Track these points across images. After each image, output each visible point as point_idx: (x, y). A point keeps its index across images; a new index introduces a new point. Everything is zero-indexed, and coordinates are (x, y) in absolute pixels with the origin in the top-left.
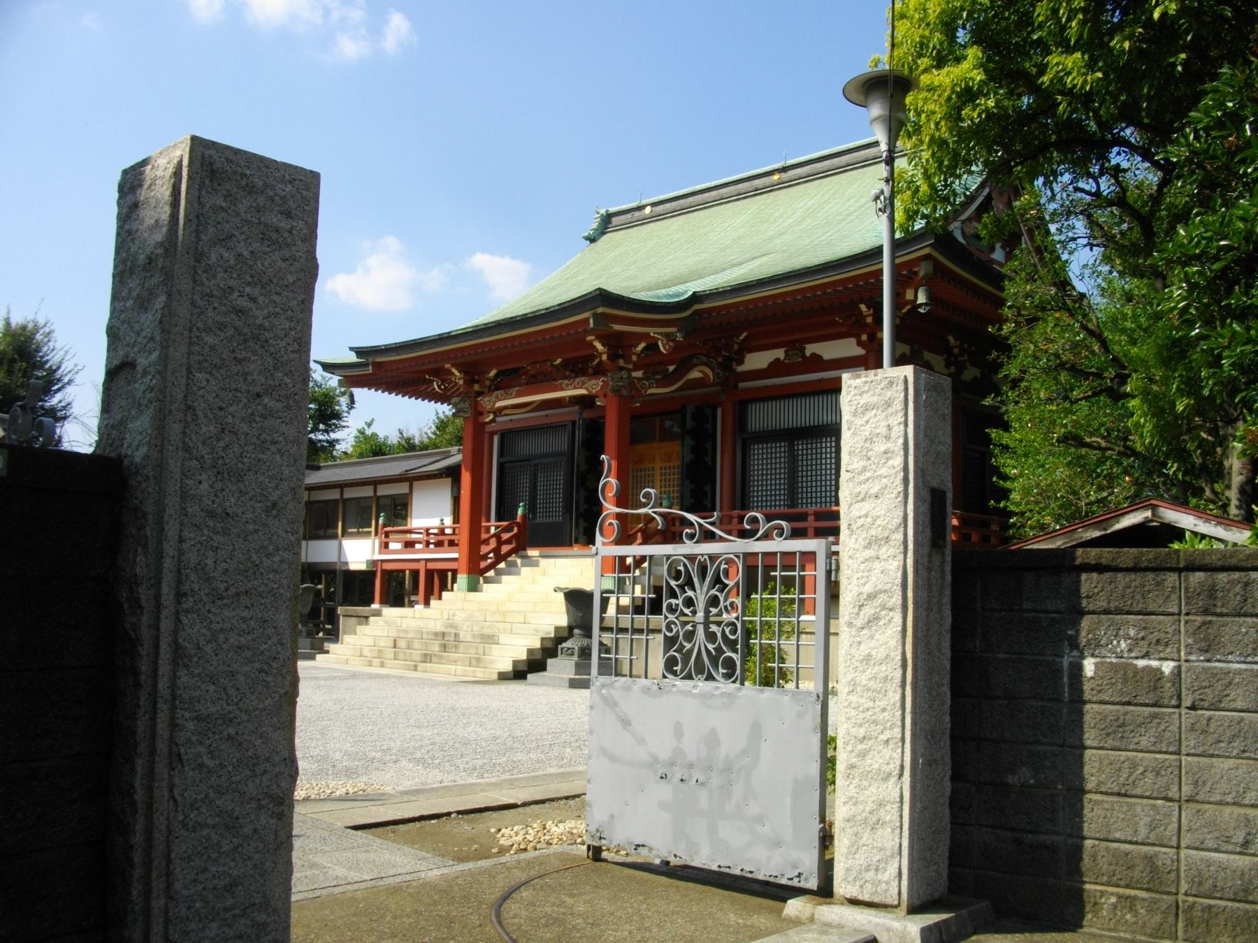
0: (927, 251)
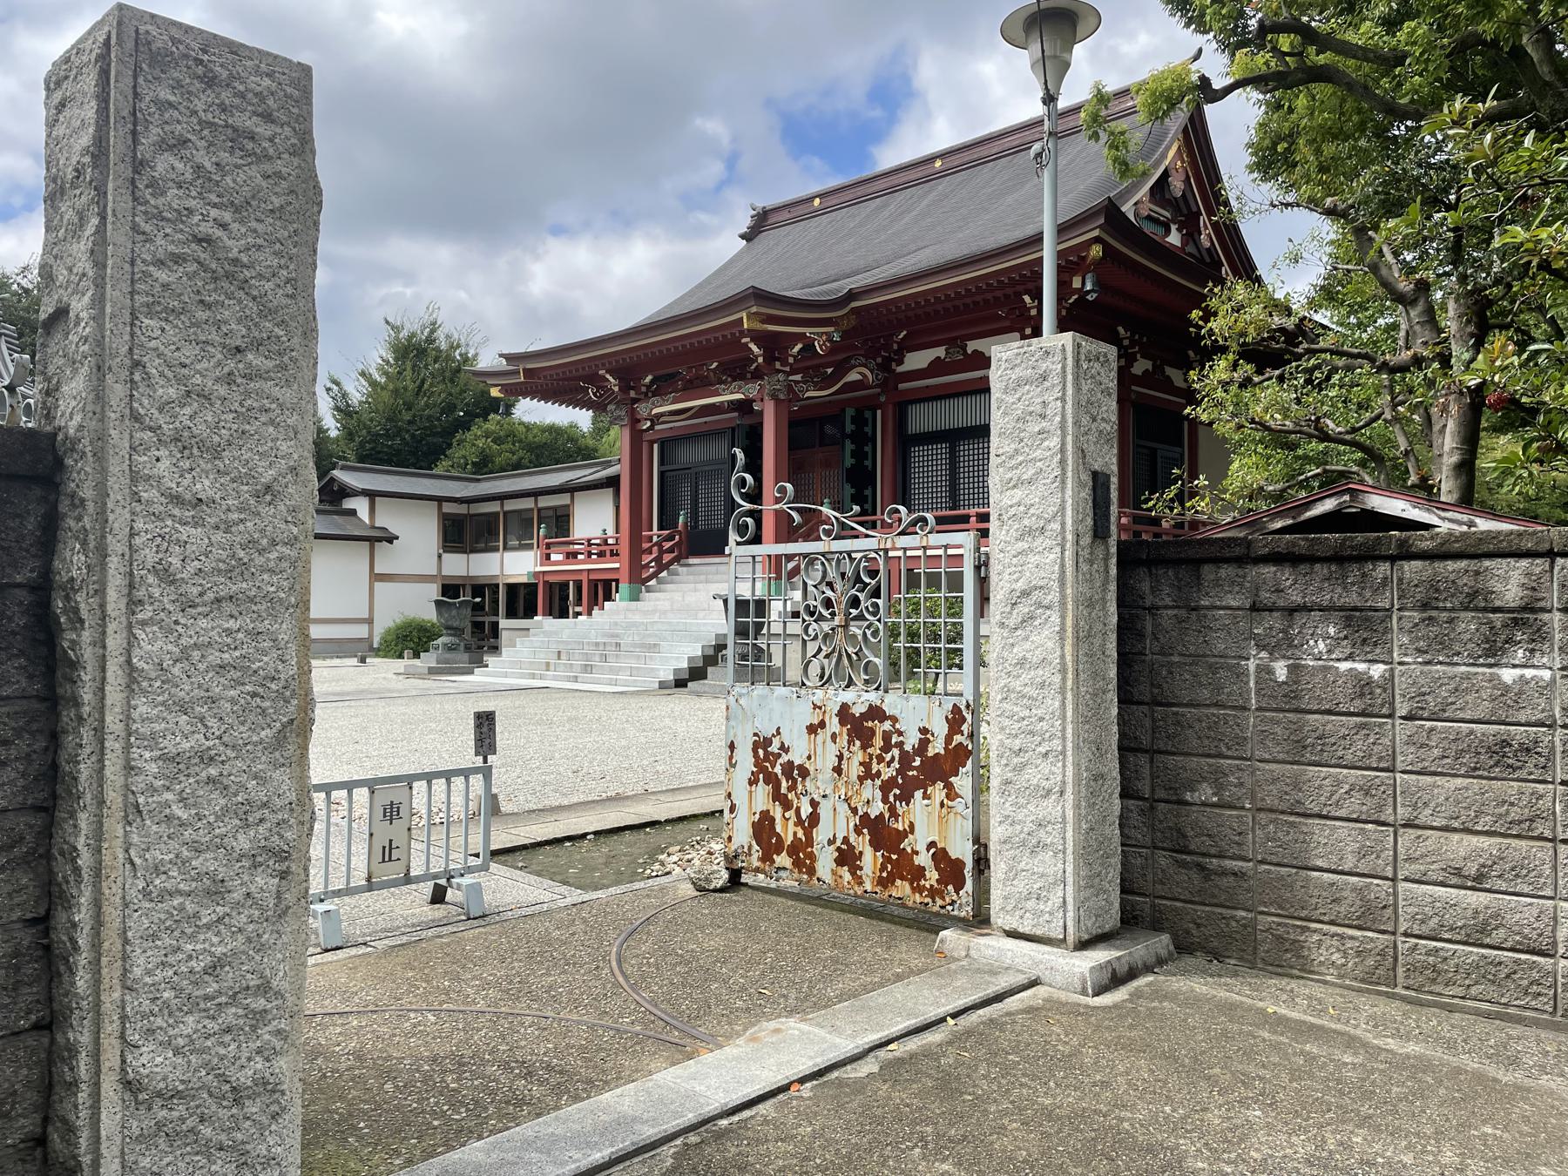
0: (1096, 233)
